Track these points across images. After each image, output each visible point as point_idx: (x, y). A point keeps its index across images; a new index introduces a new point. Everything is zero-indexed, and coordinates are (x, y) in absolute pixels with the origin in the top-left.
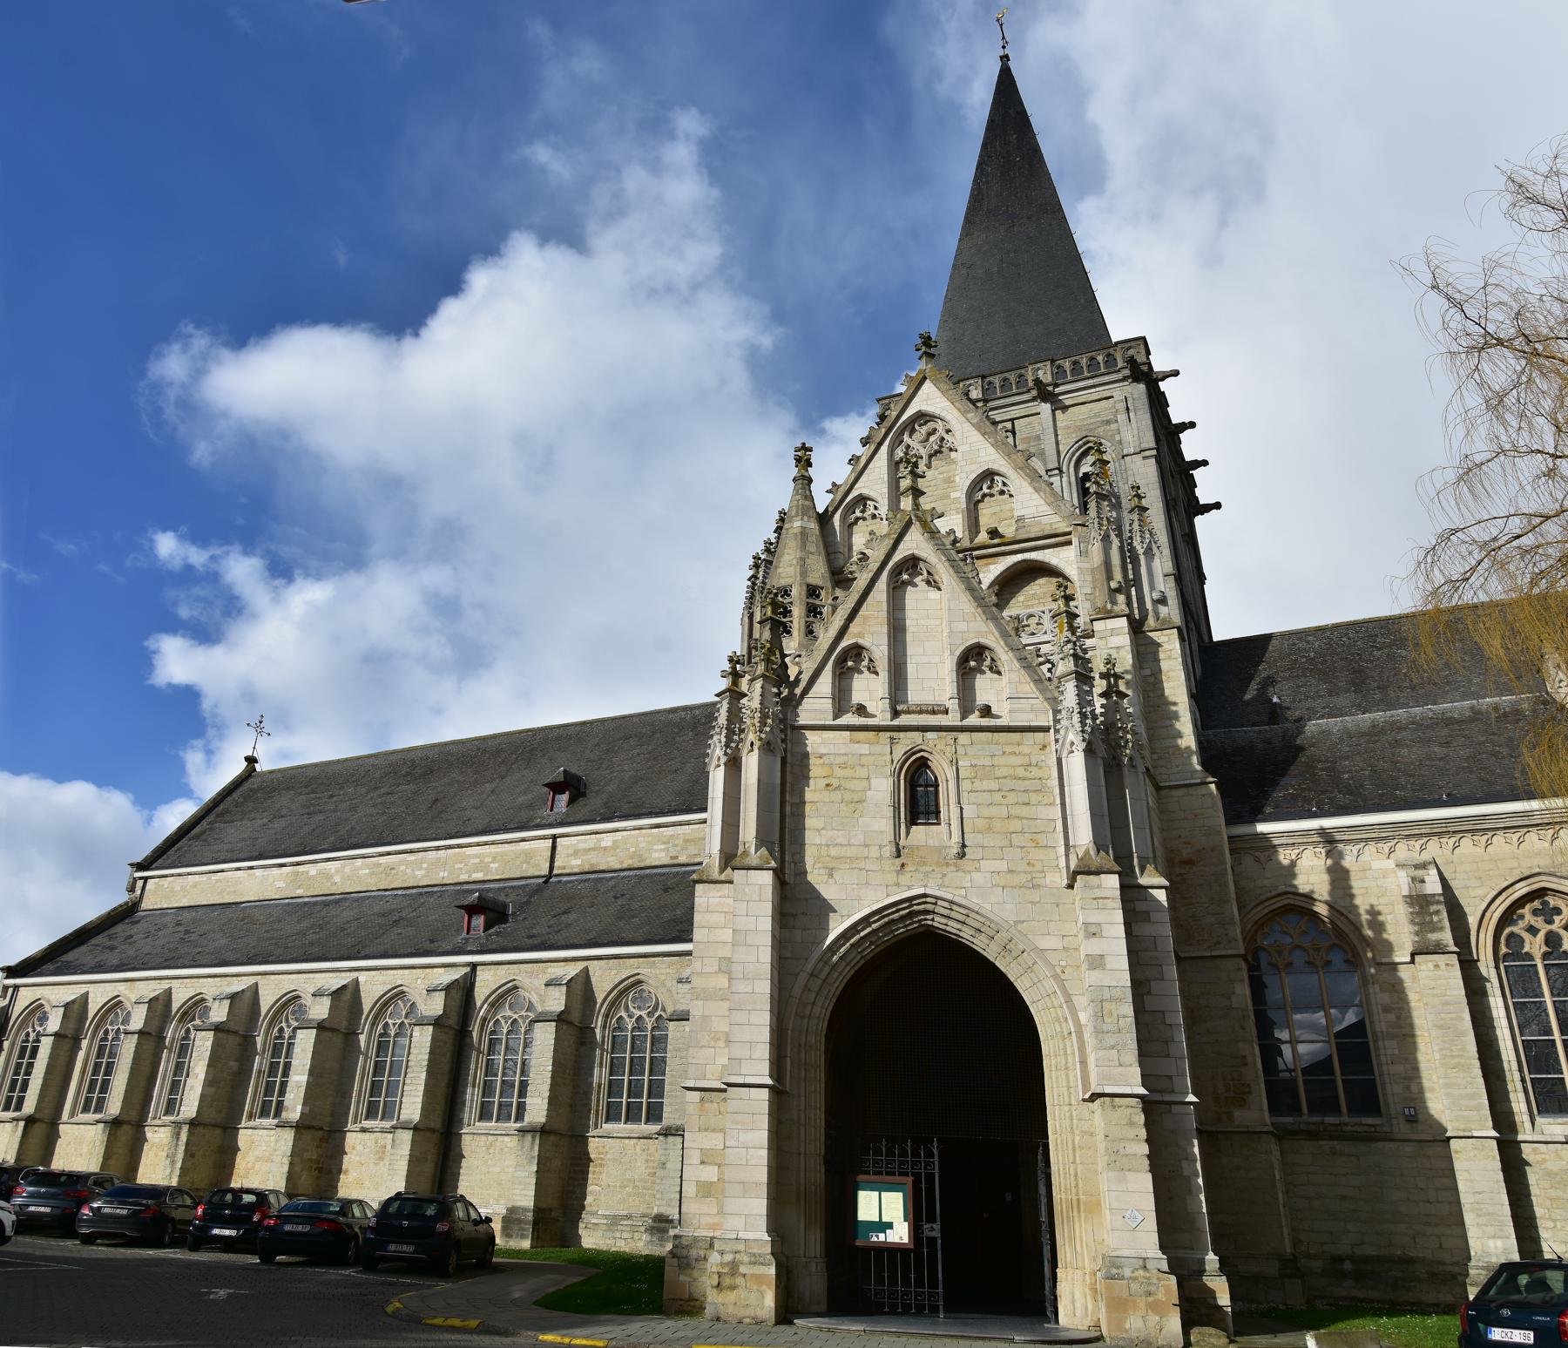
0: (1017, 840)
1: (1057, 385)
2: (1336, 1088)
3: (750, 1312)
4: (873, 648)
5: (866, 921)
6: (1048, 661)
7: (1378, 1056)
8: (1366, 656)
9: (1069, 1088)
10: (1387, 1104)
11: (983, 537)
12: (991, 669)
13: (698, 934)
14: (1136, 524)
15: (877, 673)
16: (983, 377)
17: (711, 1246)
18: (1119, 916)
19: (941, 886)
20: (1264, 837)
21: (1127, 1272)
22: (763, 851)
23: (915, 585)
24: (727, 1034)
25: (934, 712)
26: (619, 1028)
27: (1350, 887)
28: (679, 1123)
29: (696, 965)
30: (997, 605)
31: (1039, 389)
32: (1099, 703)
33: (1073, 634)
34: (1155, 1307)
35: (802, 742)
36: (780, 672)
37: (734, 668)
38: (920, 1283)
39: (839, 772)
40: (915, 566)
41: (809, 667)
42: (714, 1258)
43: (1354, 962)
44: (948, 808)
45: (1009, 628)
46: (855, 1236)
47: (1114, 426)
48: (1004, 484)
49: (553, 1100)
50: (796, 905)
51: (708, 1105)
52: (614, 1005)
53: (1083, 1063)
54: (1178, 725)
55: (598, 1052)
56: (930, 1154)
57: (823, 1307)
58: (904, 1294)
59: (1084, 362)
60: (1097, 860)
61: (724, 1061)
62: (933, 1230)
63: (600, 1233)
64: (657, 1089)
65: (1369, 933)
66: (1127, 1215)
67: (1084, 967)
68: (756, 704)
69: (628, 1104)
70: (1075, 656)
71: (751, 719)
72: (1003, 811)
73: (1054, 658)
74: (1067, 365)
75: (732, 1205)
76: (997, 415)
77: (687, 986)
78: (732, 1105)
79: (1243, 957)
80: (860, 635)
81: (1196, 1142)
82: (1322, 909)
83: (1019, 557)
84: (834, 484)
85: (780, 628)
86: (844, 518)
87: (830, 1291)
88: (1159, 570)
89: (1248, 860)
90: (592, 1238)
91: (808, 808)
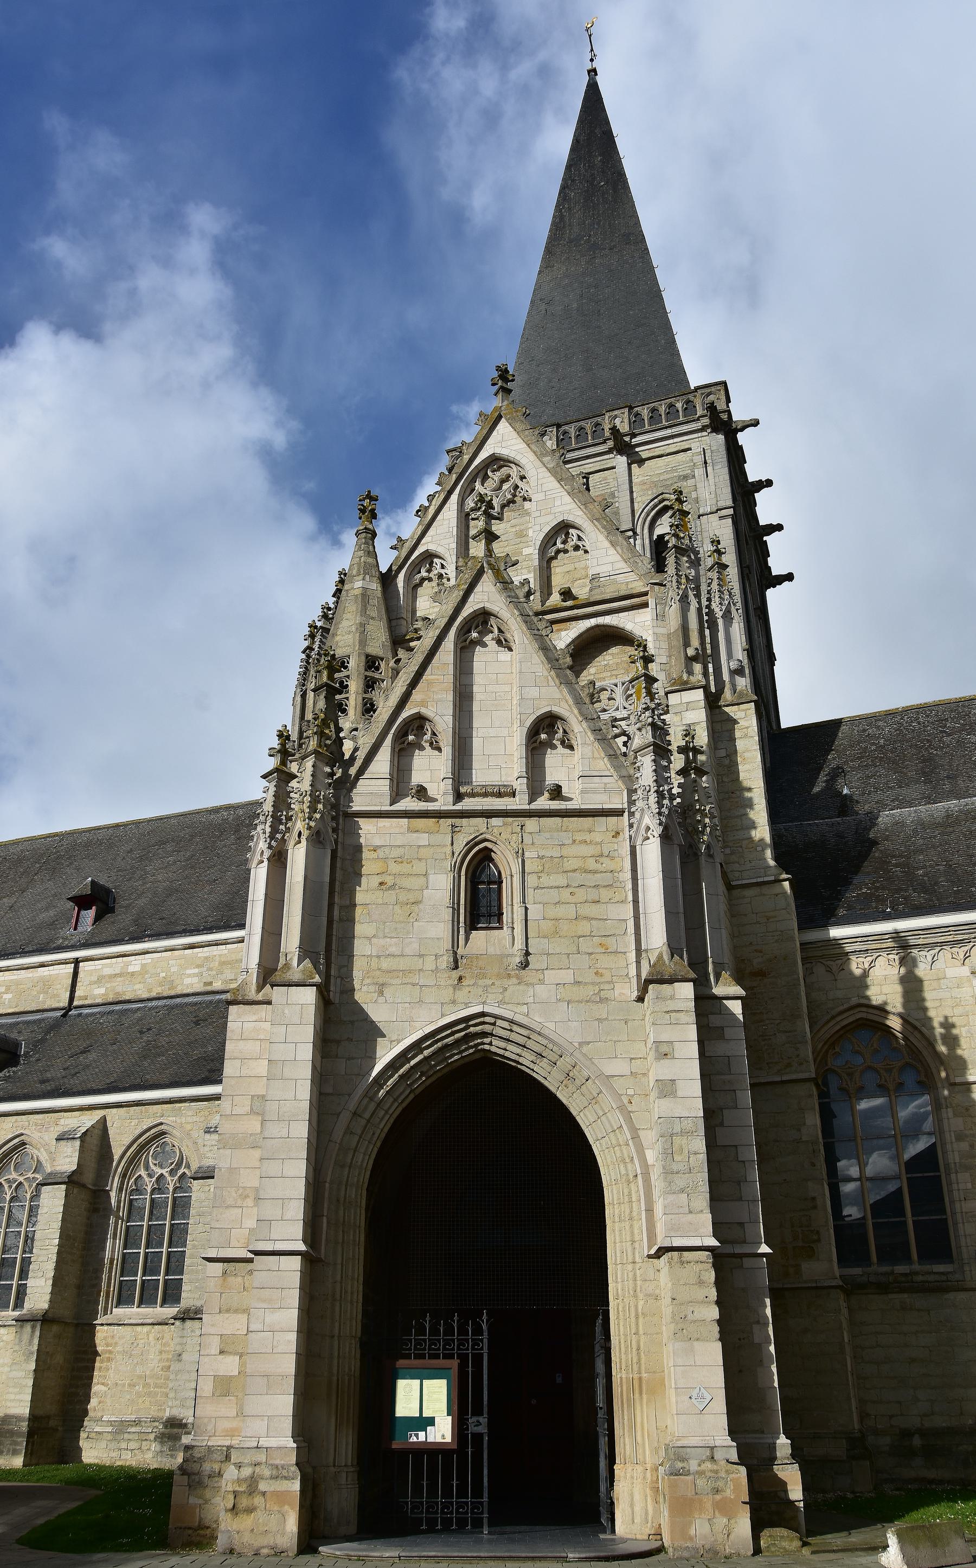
0: (585, 945)
1: (634, 435)
2: (906, 1232)
3: (268, 1540)
4: (437, 719)
5: (416, 1046)
6: (624, 733)
7: (950, 1192)
8: (936, 743)
9: (633, 1242)
10: (959, 1247)
11: (555, 599)
12: (563, 743)
13: (229, 1068)
14: (715, 582)
15: (439, 749)
16: (559, 426)
17: (228, 1458)
18: (692, 1032)
19: (501, 1003)
20: (836, 944)
21: (693, 1465)
22: (307, 963)
23: (485, 645)
24: (257, 1190)
25: (500, 795)
26: (138, 1191)
27: (924, 1000)
28: (198, 1304)
29: (225, 1104)
30: (571, 668)
31: (615, 439)
32: (676, 780)
33: (652, 700)
34: (723, 1508)
35: (354, 832)
36: (334, 748)
37: (283, 745)
38: (462, 1493)
39: (394, 868)
40: (485, 622)
41: (365, 743)
42: (231, 1473)
43: (927, 1084)
44: (512, 910)
45: (584, 695)
46: (392, 1438)
47: (691, 482)
48: (580, 538)
49: (57, 1281)
50: (341, 1028)
51: (231, 1280)
52: (133, 1162)
53: (650, 1211)
54: (752, 815)
55: (112, 1220)
56: (478, 1331)
57: (353, 1529)
58: (445, 1506)
59: (663, 409)
60: (671, 966)
61: (251, 1223)
62: (479, 1425)
63: (103, 1444)
64: (176, 1263)
65: (943, 1049)
66: (695, 1396)
67: (654, 1095)
68: (306, 786)
69: (143, 1282)
70: (653, 725)
71: (299, 805)
72: (570, 911)
73: (631, 730)
74: (645, 412)
75: (255, 1404)
76: (575, 469)
77: (215, 1137)
78: (260, 1278)
79: (814, 1081)
80: (423, 703)
81: (768, 1301)
82: (895, 1023)
83: (593, 622)
84: (400, 539)
85: (336, 709)
86: (408, 578)
87: (362, 1507)
88: (735, 641)
89: (820, 970)
90: (93, 1452)
91: (358, 911)
